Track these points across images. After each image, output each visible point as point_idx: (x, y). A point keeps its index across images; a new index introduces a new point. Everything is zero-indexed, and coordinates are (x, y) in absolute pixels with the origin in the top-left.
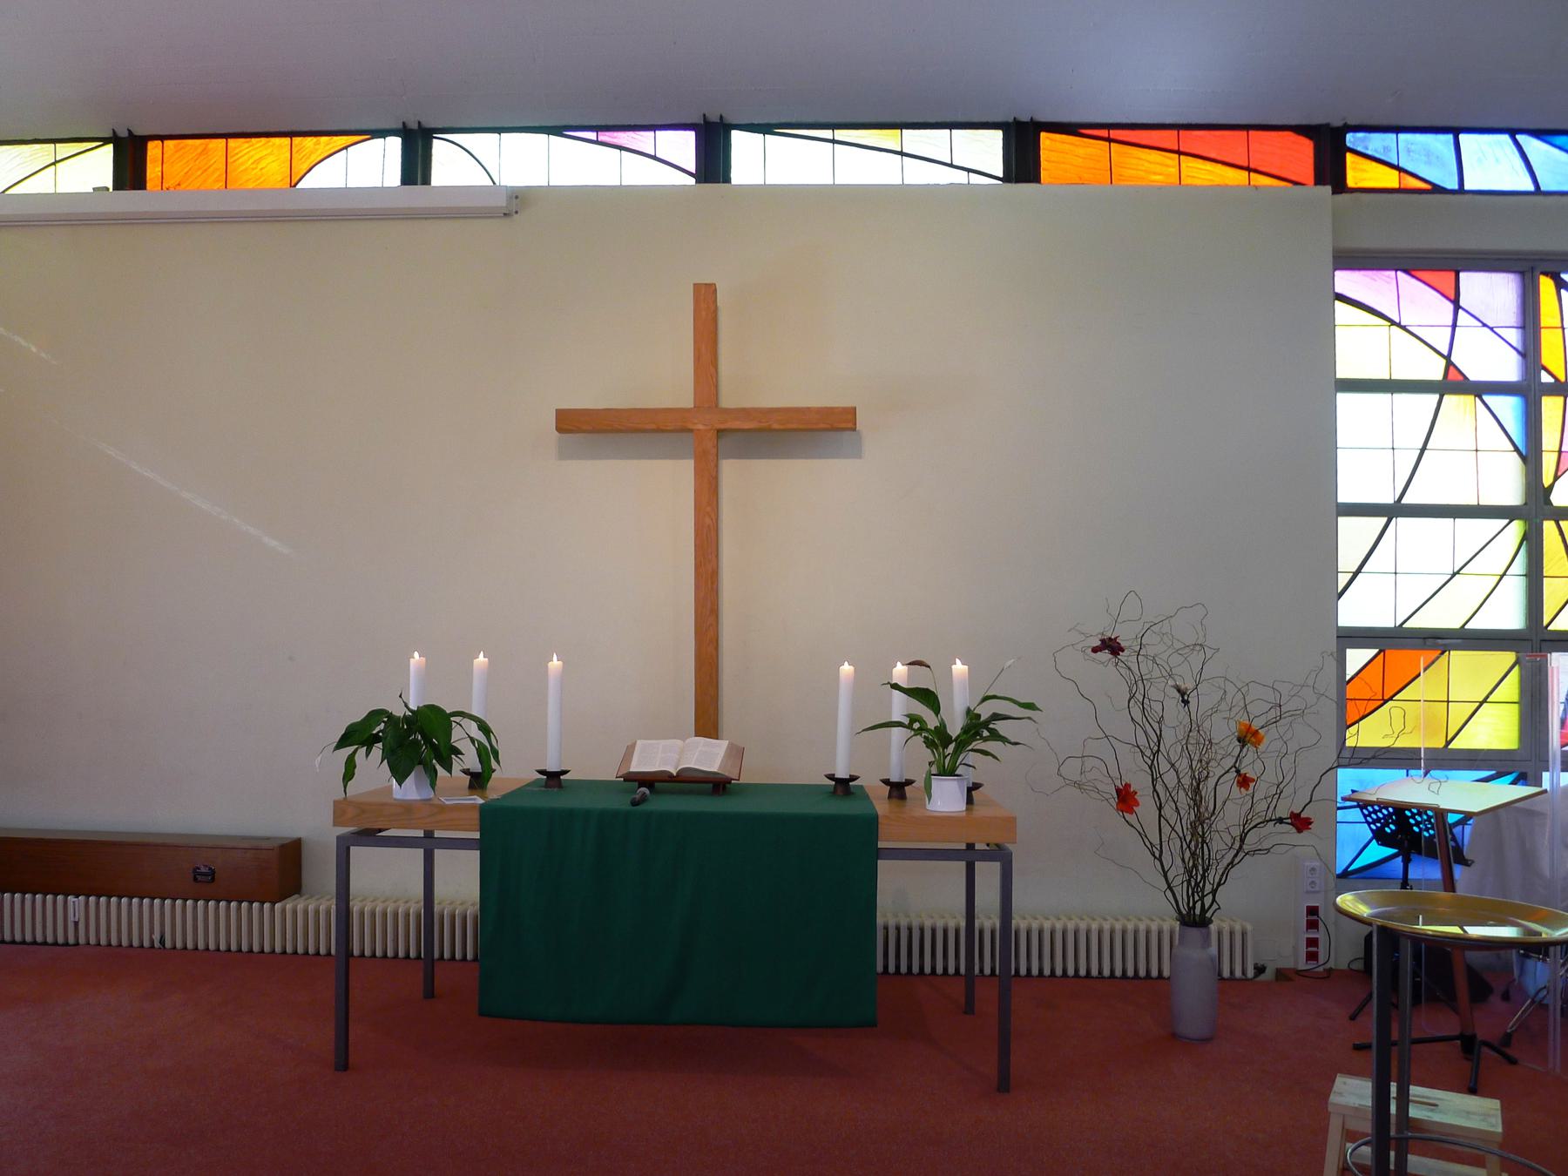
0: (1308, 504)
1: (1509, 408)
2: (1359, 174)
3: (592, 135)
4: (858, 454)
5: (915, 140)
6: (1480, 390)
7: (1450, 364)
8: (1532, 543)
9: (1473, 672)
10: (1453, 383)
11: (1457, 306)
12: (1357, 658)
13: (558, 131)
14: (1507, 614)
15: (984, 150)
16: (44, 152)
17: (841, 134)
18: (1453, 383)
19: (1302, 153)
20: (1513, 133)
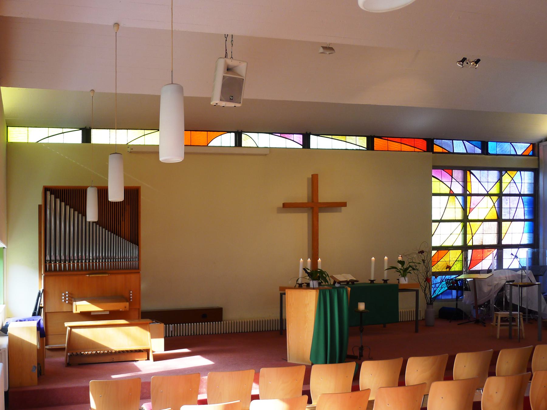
0: (425, 222)
1: (460, 198)
2: (437, 149)
3: (279, 135)
4: (341, 212)
5: (349, 139)
6: (456, 195)
7: (451, 190)
8: (465, 228)
9: (455, 255)
10: (452, 194)
11: (452, 177)
12: (434, 252)
13: (272, 134)
14: (459, 243)
15: (362, 142)
16: (141, 132)
17: (333, 137)
18: (452, 194)
19: (423, 144)
20: (463, 141)
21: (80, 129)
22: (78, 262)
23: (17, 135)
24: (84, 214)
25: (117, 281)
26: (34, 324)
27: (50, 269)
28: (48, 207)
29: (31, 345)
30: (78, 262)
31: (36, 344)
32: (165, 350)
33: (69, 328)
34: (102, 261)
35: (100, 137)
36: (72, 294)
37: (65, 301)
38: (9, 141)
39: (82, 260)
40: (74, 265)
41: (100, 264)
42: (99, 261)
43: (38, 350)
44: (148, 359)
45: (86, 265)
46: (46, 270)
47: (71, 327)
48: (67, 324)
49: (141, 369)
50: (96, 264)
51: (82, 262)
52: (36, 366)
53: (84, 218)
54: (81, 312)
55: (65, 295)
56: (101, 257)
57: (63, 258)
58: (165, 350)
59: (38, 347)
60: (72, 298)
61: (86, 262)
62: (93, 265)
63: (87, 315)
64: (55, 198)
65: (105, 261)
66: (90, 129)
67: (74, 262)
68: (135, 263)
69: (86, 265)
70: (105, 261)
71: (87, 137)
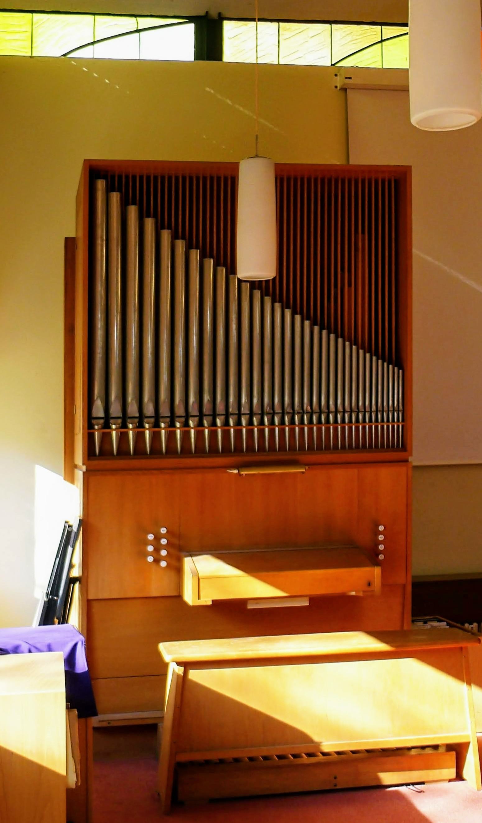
16: (373, 32)
21: (190, 19)
22: (200, 424)
25: (327, 492)
26: (54, 667)
28: (101, 232)
29: (39, 772)
30: (200, 424)
31: (62, 771)
33: (180, 670)
34: (282, 422)
36: (179, 537)
37: (157, 561)
40: (186, 435)
41: (272, 431)
42: (272, 422)
43: (70, 792)
45: (226, 434)
46: (90, 453)
47: (187, 665)
48: (173, 652)
51: (214, 424)
54: (217, 605)
55: (158, 538)
56: (278, 409)
57: (149, 409)
59: (72, 780)
60: (182, 547)
63: (234, 617)
65: (292, 422)
66: (221, 18)
67: (186, 424)
68: (390, 427)
70: (292, 422)
71: (209, 44)
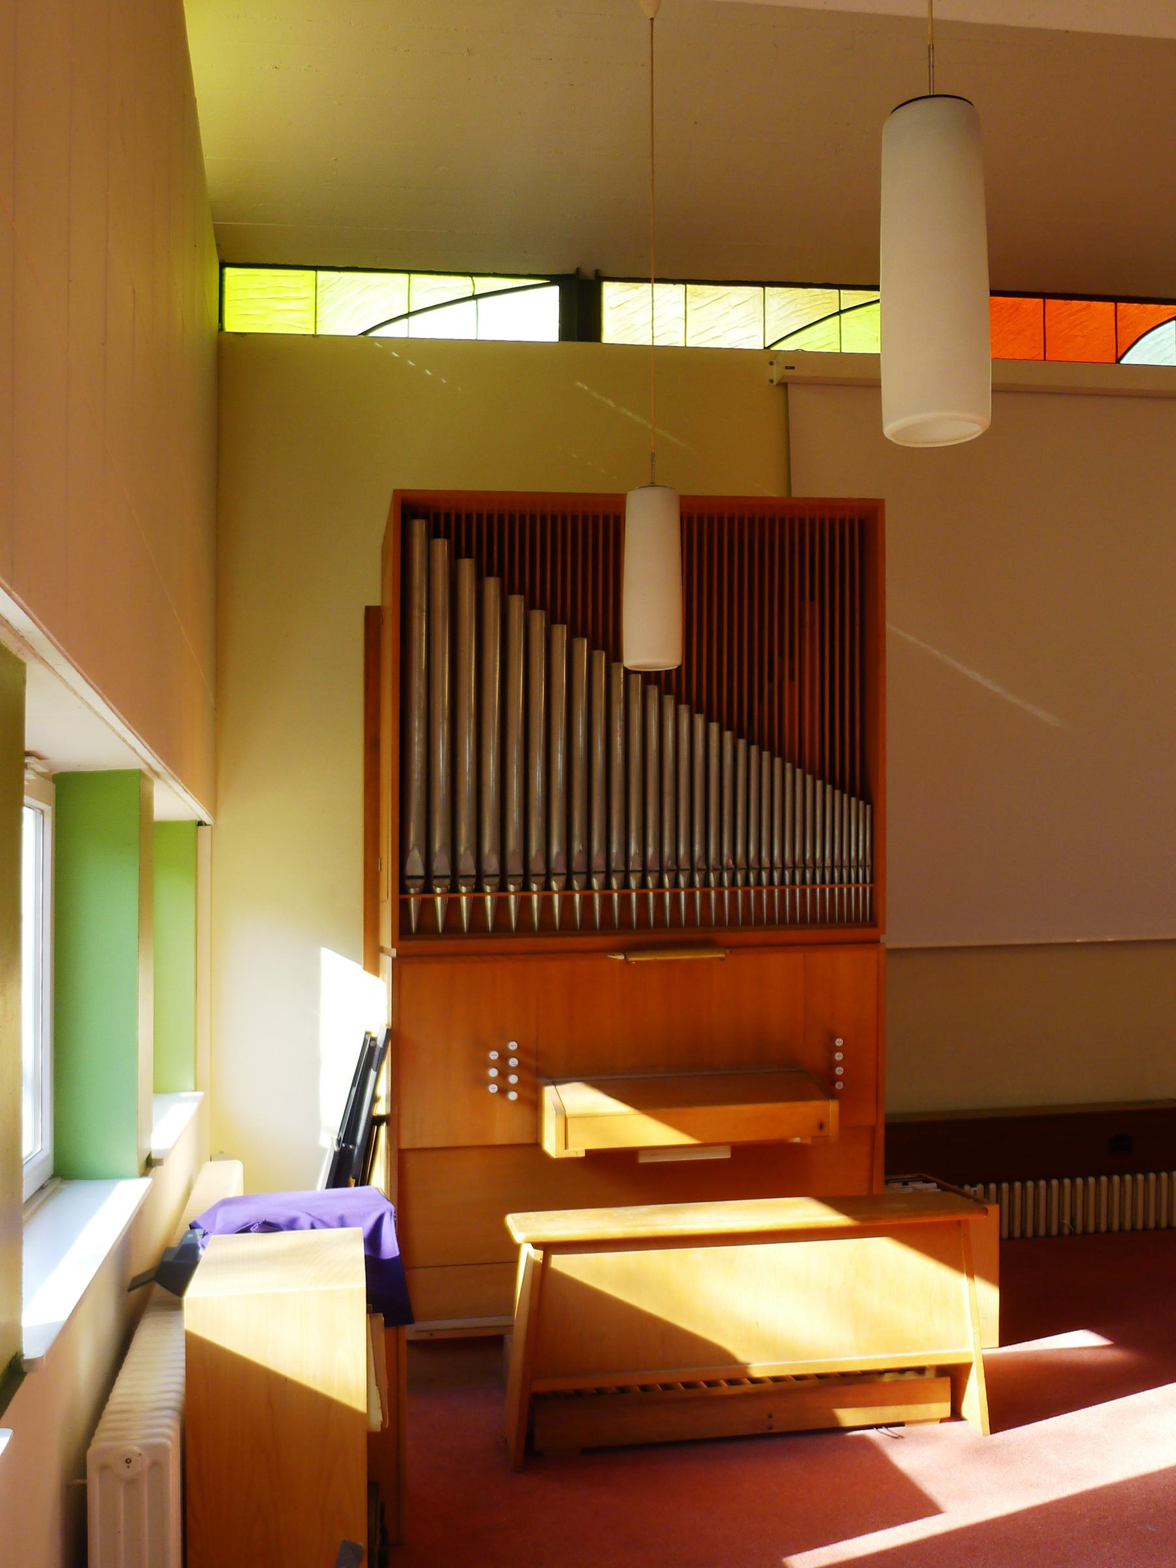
16: (827, 299)
21: (553, 280)
22: (568, 886)
23: (264, 303)
24: (607, 637)
25: (758, 988)
27: (434, 917)
29: (323, 1407)
30: (568, 886)
32: (1002, 1345)
33: (538, 1255)
34: (691, 883)
35: (637, 314)
37: (503, 1091)
38: (231, 325)
39: (627, 873)
40: (546, 903)
41: (675, 896)
42: (675, 884)
43: (372, 1437)
44: (956, 1415)
45: (607, 901)
46: (402, 931)
47: (549, 1248)
49: (932, 1488)
50: (660, 899)
51: (588, 886)
52: (362, 1543)
53: (601, 657)
54: (594, 1156)
55: (504, 1056)
58: (1002, 1345)
59: (377, 1420)
60: (541, 1071)
61: (607, 885)
62: (643, 899)
63: (618, 1175)
64: (455, 555)
65: (706, 883)
67: (547, 887)
69: (607, 901)
71: (581, 317)
